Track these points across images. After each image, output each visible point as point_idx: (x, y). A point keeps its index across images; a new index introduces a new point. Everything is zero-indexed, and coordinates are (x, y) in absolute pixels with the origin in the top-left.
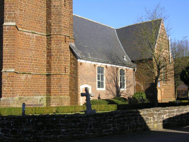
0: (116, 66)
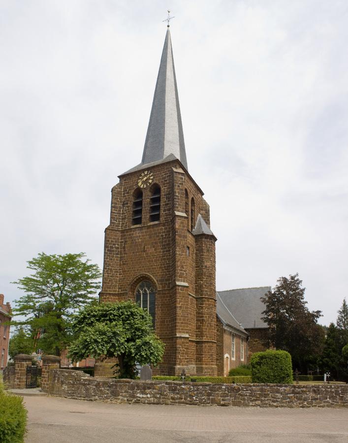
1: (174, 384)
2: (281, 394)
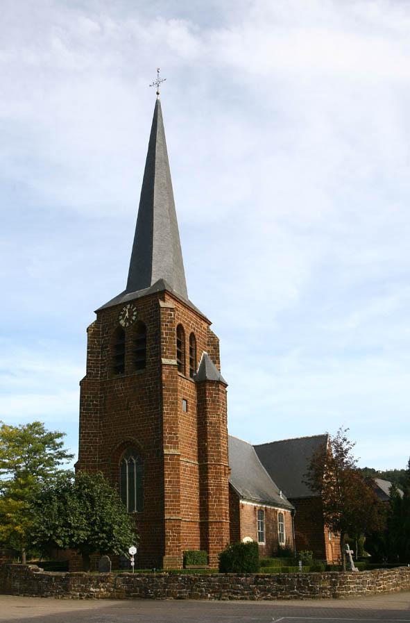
0: (272, 508)
2: (242, 584)
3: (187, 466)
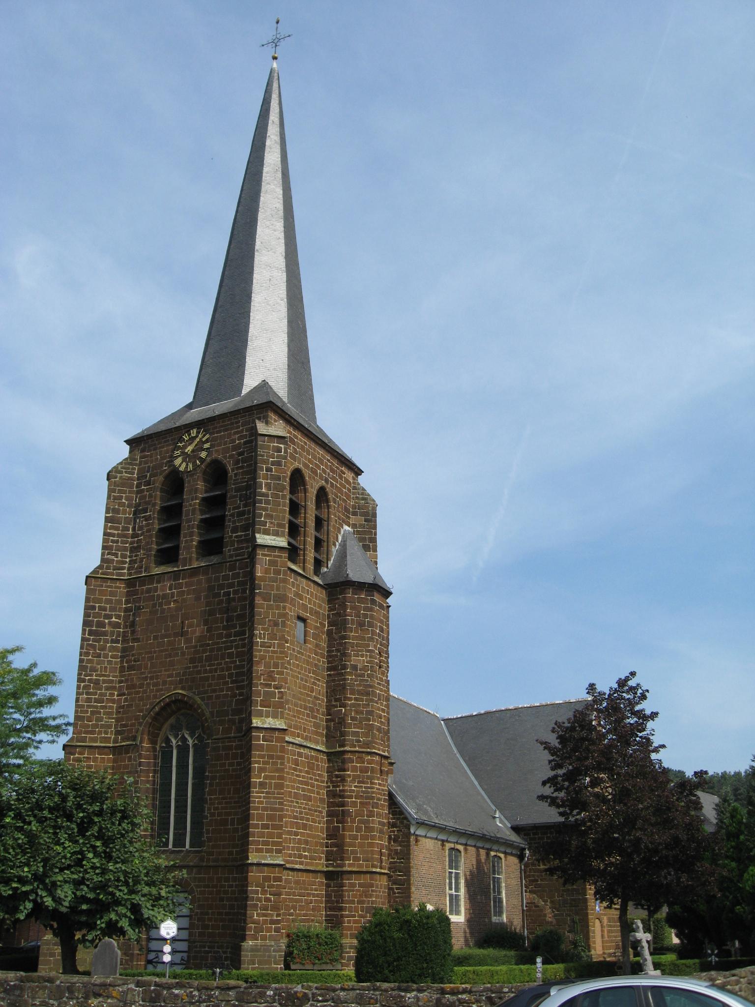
1: (156, 985)
3: (300, 755)
